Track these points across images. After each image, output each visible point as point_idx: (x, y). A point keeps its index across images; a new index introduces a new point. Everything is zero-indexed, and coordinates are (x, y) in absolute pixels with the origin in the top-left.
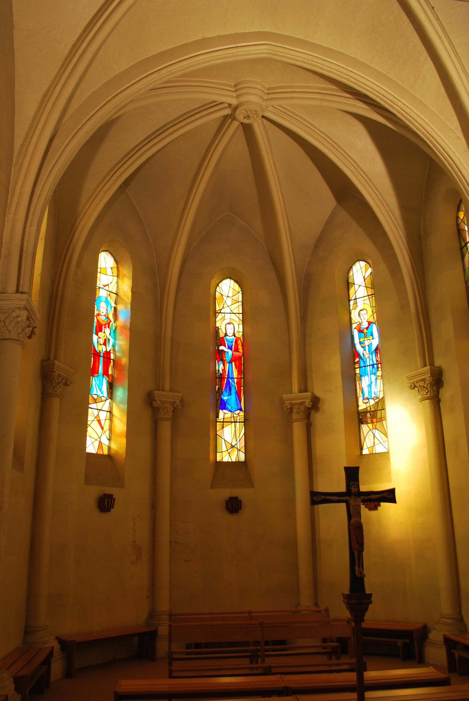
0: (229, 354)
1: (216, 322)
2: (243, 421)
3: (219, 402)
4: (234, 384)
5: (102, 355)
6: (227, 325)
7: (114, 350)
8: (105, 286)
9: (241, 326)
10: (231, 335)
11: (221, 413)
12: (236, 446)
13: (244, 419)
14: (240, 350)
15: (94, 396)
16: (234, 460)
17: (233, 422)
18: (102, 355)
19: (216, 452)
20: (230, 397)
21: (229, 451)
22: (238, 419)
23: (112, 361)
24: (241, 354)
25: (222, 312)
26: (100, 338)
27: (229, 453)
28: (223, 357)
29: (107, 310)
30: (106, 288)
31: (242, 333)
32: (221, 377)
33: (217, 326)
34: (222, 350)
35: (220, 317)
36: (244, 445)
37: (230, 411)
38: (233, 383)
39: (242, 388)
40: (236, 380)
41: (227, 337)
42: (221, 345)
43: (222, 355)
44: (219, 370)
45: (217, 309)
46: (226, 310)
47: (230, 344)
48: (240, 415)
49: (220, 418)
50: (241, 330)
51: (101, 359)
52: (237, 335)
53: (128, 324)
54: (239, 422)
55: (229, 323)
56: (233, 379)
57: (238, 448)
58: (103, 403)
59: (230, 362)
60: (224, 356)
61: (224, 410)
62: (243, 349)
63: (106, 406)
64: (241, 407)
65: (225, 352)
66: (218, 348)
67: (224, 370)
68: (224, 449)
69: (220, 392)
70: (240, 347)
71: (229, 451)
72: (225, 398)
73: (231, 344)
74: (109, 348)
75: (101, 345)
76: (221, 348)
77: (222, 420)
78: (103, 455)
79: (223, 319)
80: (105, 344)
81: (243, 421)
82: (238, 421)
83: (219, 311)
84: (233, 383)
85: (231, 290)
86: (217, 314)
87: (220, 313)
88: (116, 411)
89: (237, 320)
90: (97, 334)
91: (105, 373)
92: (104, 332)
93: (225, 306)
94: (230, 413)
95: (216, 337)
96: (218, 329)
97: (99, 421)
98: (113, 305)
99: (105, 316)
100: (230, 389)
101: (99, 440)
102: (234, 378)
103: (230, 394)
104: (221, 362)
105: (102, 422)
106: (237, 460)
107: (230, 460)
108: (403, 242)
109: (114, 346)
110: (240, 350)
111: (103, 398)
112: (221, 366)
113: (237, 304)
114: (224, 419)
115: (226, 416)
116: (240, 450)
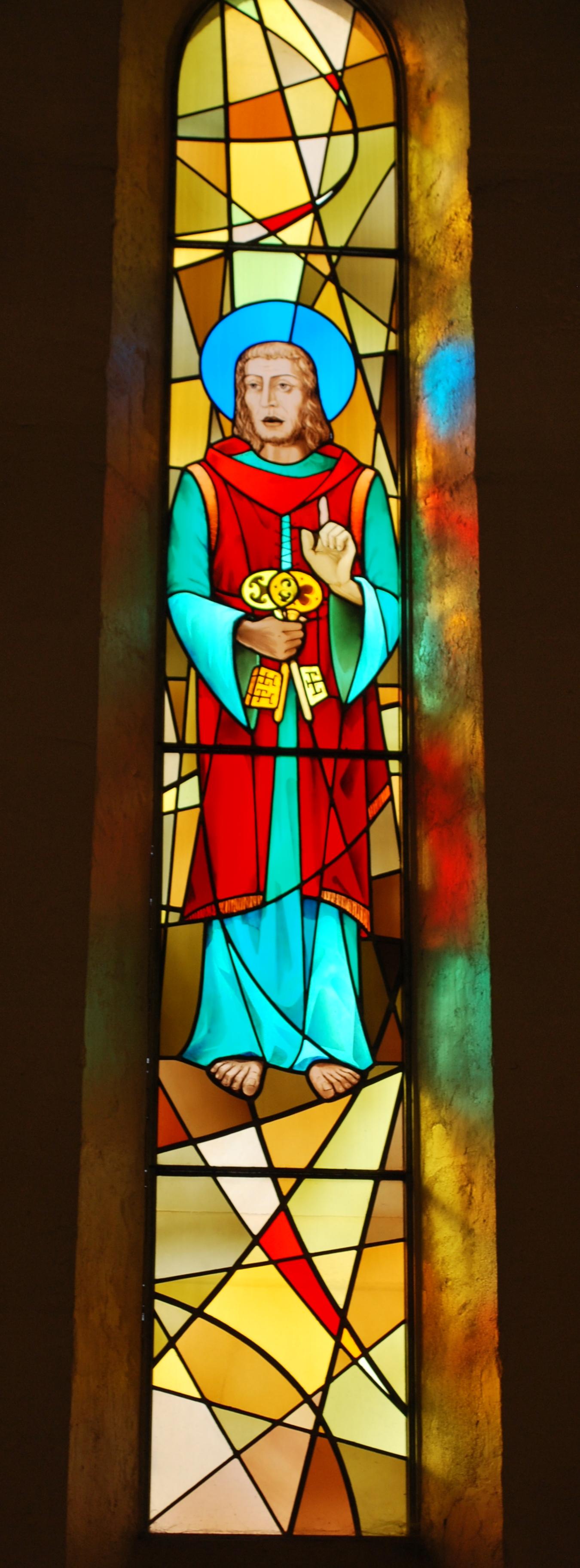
5: (288, 738)
7: (407, 684)
8: (276, 223)
15: (229, 1071)
18: (288, 738)
19: (243, 913)
23: (394, 766)
26: (256, 615)
29: (314, 393)
30: (299, 233)
34: (311, 421)
51: (286, 770)
53: (468, 464)
58: (329, 1112)
63: (367, 1130)
74: (362, 668)
75: (275, 665)
78: (359, 1546)
80: (313, 647)
88: (440, 1161)
90: (223, 591)
91: (331, 872)
92: (301, 564)
97: (297, 1267)
98: (373, 338)
99: (297, 438)
101: (305, 1417)
105: (335, 1273)
109: (403, 649)
111: (316, 1073)
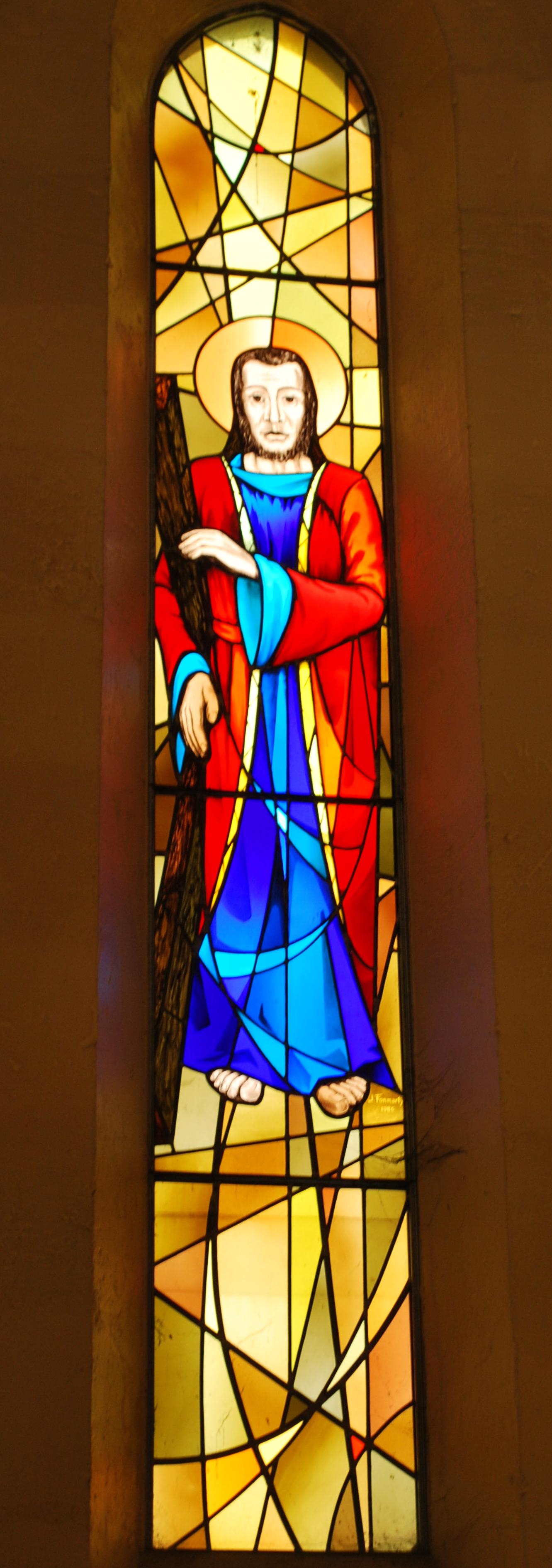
0: (269, 599)
1: (151, 335)
2: (398, 1171)
3: (179, 996)
4: (311, 846)
6: (253, 370)
9: (368, 383)
10: (288, 444)
11: (197, 1102)
12: (333, 1405)
13: (410, 1157)
14: (366, 570)
16: (314, 1539)
17: (303, 1183)
19: (144, 1461)
20: (278, 956)
21: (269, 1450)
22: (352, 1153)
24: (372, 603)
25: (203, 259)
27: (269, 1472)
28: (209, 617)
31: (374, 440)
32: (196, 785)
33: (163, 366)
35: (185, 298)
36: (407, 1396)
37: (272, 1079)
38: (302, 841)
39: (385, 885)
40: (325, 816)
41: (249, 460)
42: (198, 523)
43: (207, 605)
44: (174, 724)
45: (167, 232)
46: (247, 249)
47: (272, 514)
48: (369, 1117)
49: (181, 1141)
50: (369, 408)
52: (335, 449)
54: (364, 1184)
55: (269, 354)
56: (302, 810)
57: (358, 1424)
59: (279, 664)
60: (219, 610)
61: (221, 1077)
62: (388, 561)
64: (378, 1049)
65: (233, 576)
66: (173, 541)
67: (221, 729)
68: (222, 1427)
69: (185, 917)
70: (361, 541)
71: (269, 1450)
72: (232, 966)
73: (290, 514)
76: (202, 543)
77: (204, 1164)
79: (219, 314)
81: (398, 1171)
82: (352, 1172)
83: (181, 255)
84: (302, 841)
85: (284, 105)
86: (163, 277)
87: (191, 266)
89: (335, 329)
93: (233, 216)
94: (275, 1098)
95: (156, 457)
96: (174, 391)
100: (279, 894)
102: (313, 800)
103: (275, 936)
104: (193, 662)
106: (347, 1540)
107: (276, 1540)
108: (271, 646)
110: (366, 570)
112: (199, 694)
113: (336, 213)
114: (219, 1147)
115: (245, 1125)
116: (369, 1444)
